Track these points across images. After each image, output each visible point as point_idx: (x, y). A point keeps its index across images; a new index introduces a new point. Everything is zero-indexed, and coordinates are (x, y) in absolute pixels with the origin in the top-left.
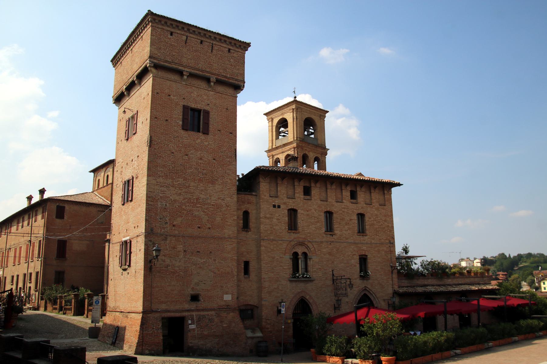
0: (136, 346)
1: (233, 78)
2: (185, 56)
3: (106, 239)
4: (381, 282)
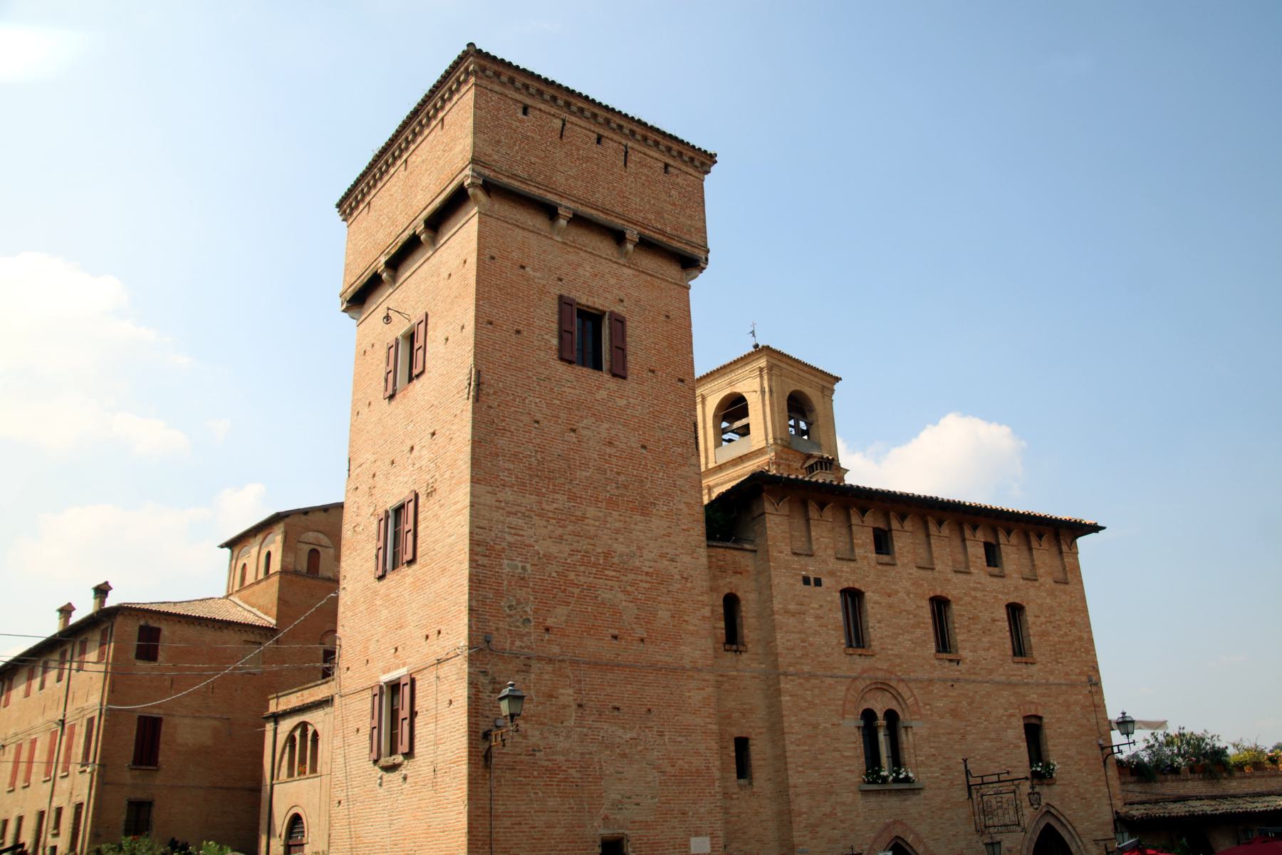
3: (266, 714)
4: (1082, 791)
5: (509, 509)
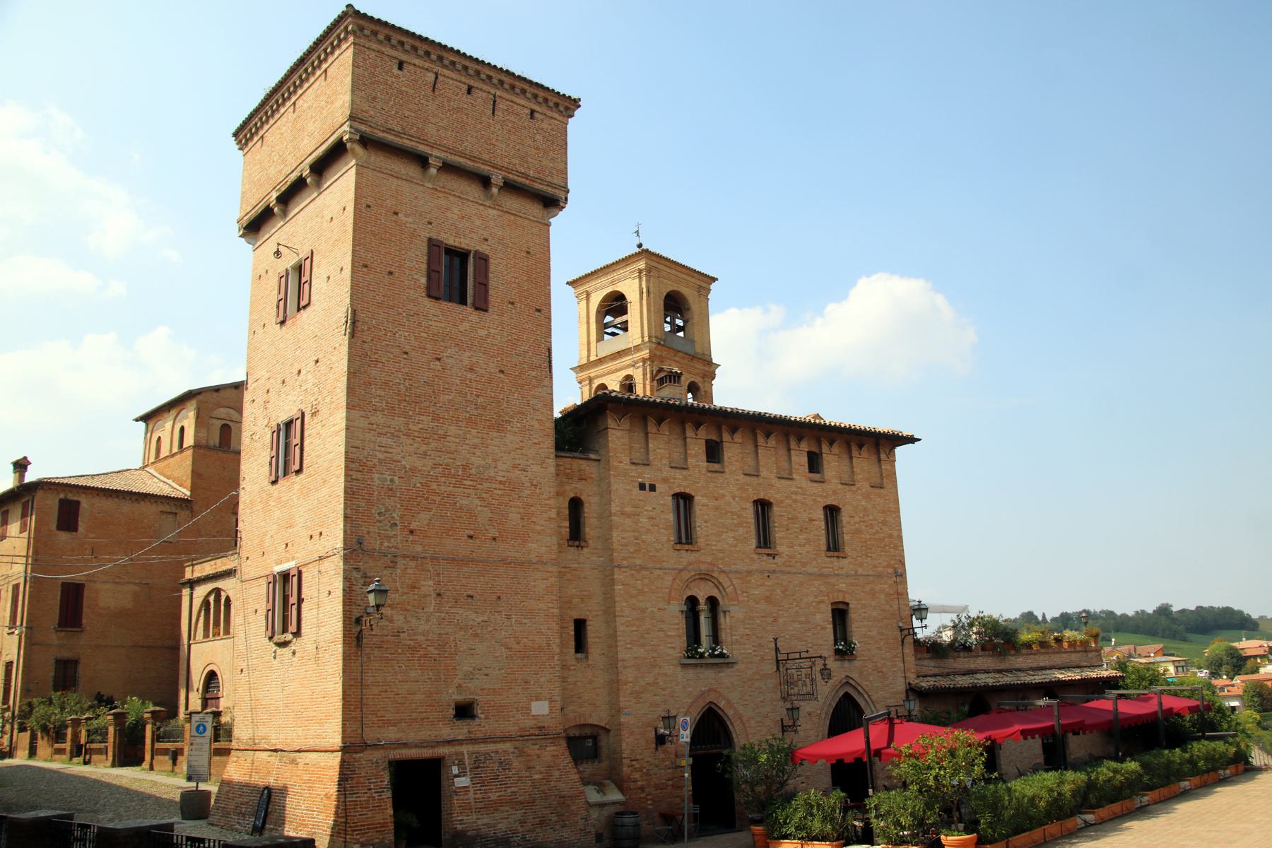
0: (331, 835)
1: (542, 180)
2: (432, 121)
3: (183, 580)
4: (879, 665)
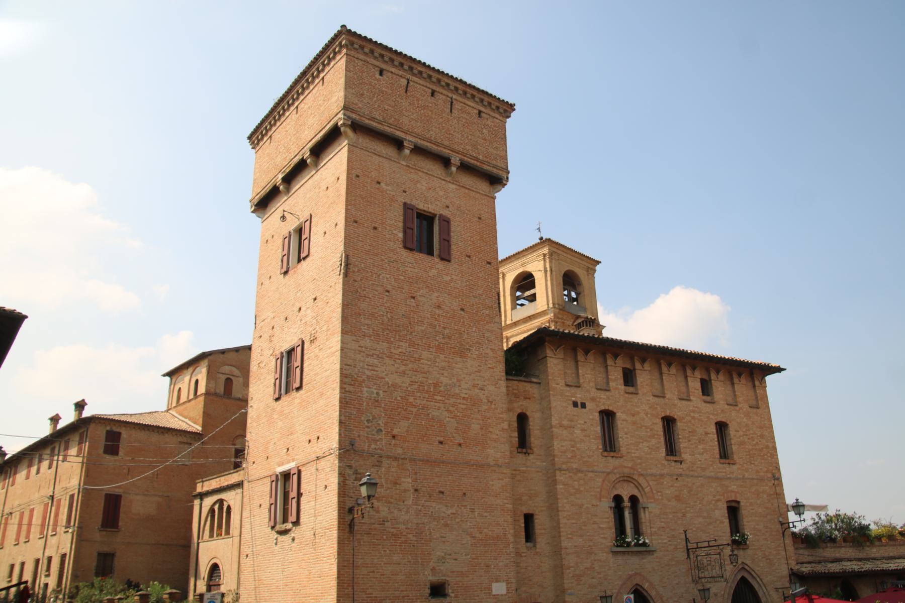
3: (195, 493)
4: (767, 553)
5: (368, 353)
